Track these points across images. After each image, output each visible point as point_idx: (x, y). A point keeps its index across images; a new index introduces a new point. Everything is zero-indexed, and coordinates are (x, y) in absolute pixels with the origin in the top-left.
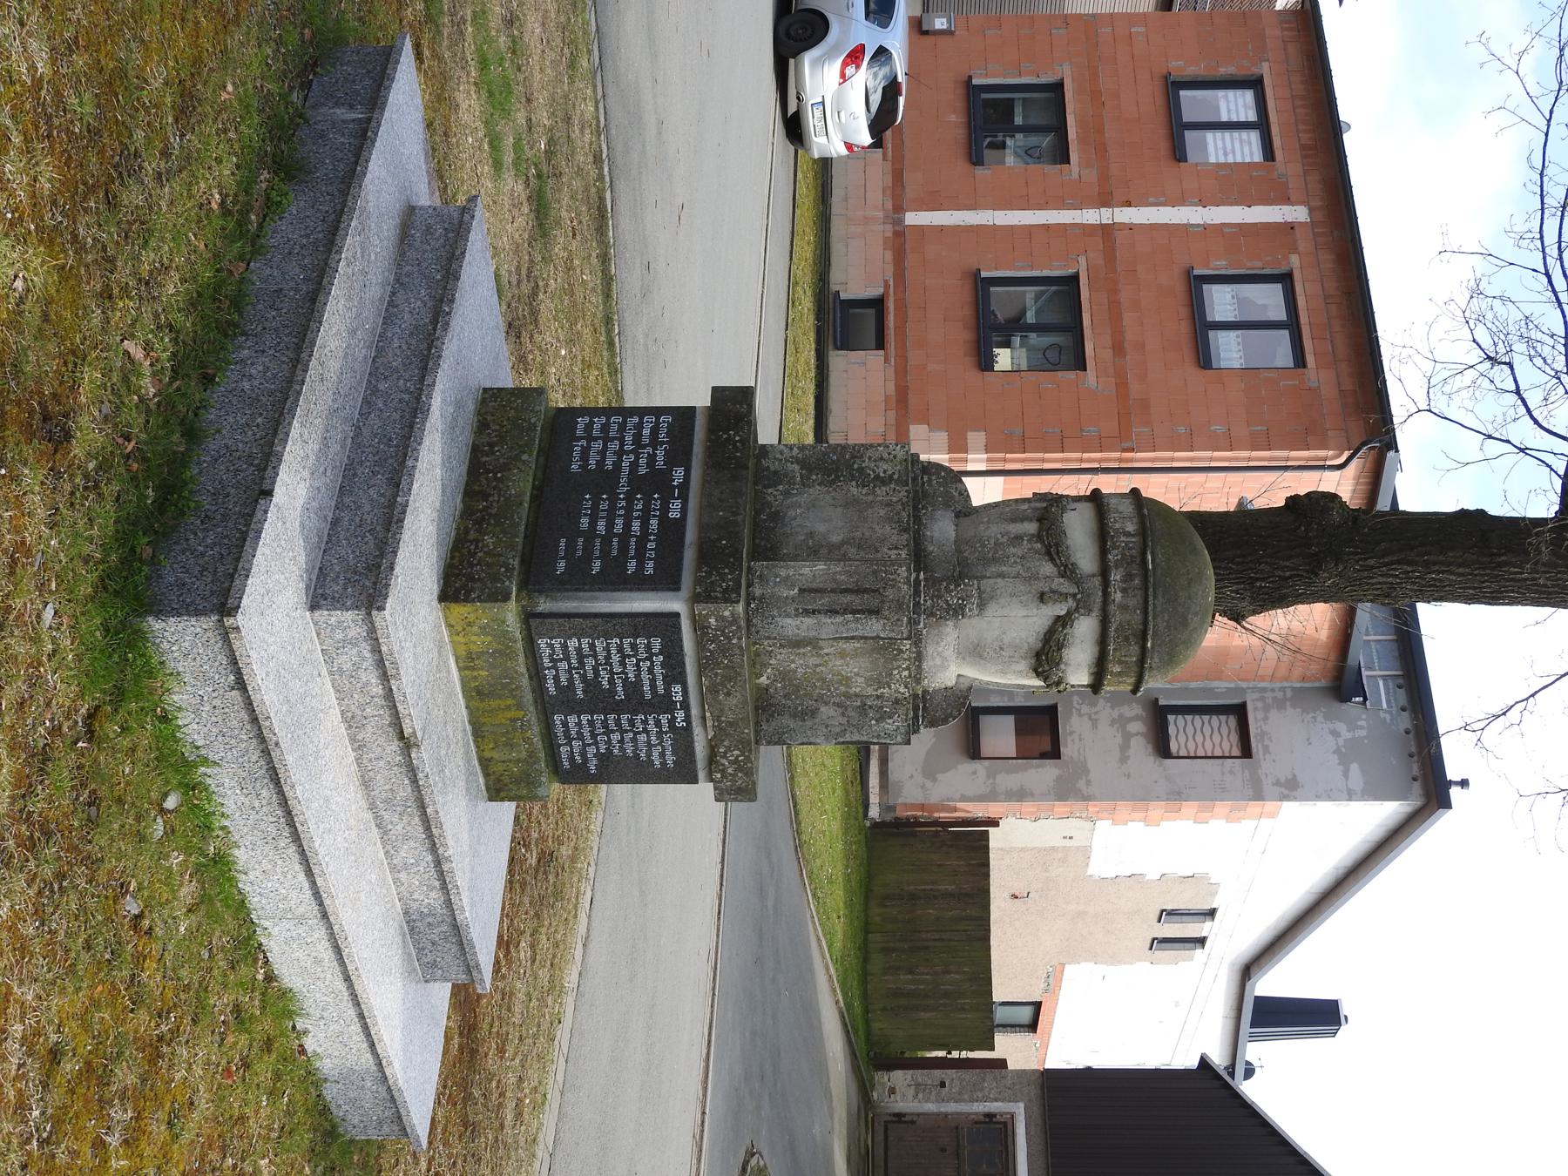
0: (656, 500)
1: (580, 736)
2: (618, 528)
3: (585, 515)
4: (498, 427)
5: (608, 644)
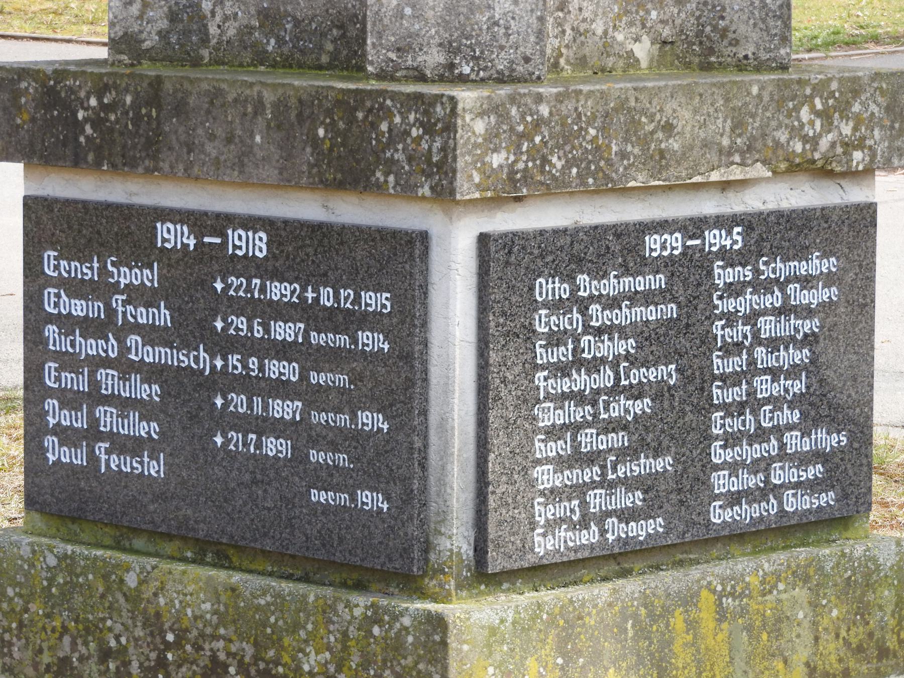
0: (228, 287)
1: (762, 465)
2: (289, 371)
3: (258, 446)
4: (67, 640)
5: (548, 397)
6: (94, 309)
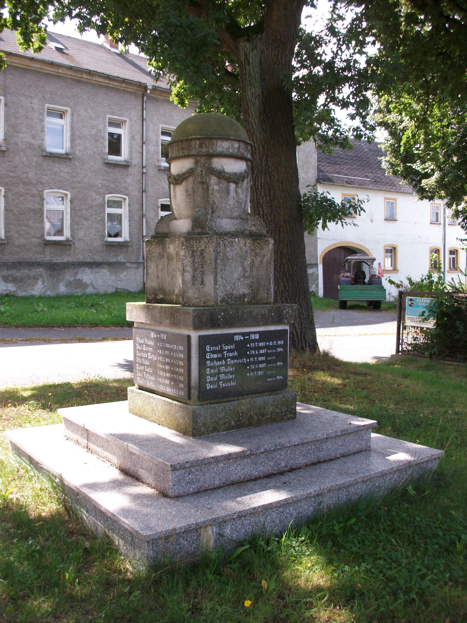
2: (263, 358)
6: (220, 355)
